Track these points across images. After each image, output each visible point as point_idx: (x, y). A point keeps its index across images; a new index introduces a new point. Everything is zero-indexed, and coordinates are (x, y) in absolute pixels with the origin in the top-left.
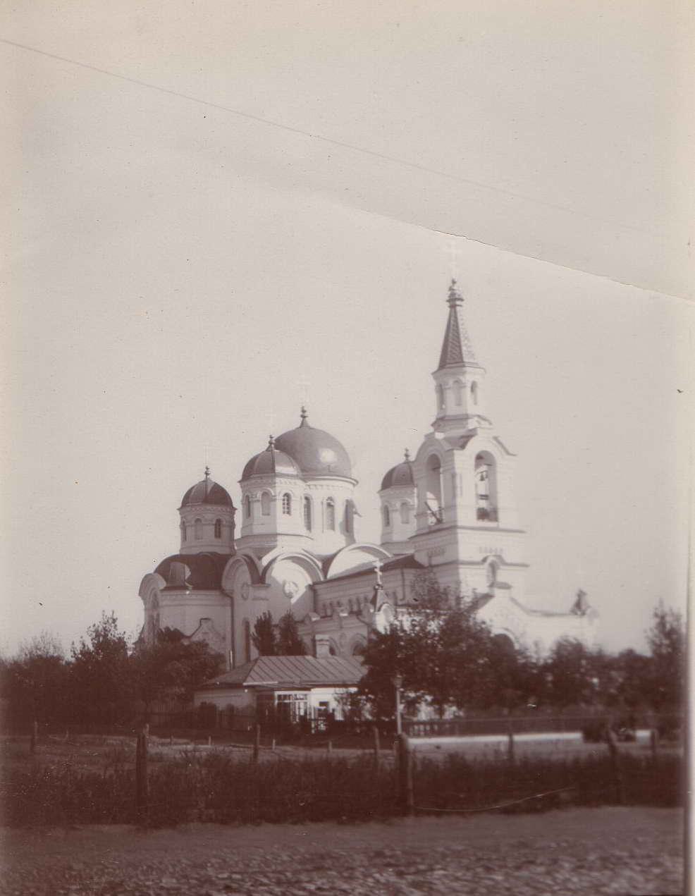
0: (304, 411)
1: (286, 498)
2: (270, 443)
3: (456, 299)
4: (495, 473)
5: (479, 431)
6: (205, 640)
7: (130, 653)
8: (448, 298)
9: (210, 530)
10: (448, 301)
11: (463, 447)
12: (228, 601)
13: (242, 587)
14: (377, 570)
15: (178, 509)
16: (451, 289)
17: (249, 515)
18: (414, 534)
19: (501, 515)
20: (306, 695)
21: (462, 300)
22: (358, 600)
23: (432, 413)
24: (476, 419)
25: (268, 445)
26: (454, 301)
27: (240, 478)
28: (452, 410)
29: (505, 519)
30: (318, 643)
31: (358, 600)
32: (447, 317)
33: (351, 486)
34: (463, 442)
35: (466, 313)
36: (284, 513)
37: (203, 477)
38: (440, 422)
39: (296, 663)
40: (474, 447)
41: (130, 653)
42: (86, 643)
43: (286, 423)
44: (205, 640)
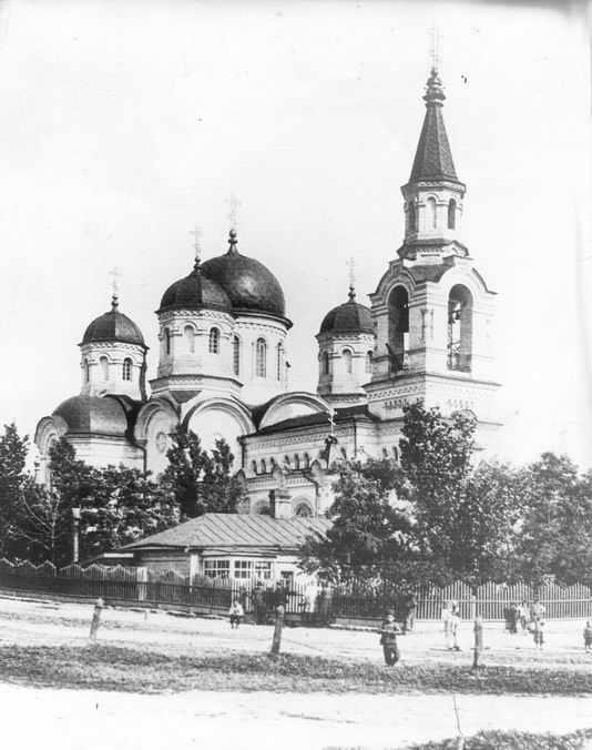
0: (232, 236)
3: (437, 96)
4: (469, 314)
5: (456, 260)
6: (577, 466)
8: (424, 94)
9: (118, 370)
10: (425, 98)
11: (437, 279)
12: (140, 453)
13: (158, 437)
14: (331, 420)
15: (157, 312)
17: (168, 352)
18: (369, 381)
19: (474, 363)
20: (269, 563)
21: (443, 98)
24: (453, 246)
25: (193, 269)
26: (433, 98)
27: (158, 307)
28: (426, 231)
30: (277, 500)
33: (284, 328)
34: (436, 274)
35: (449, 113)
36: (210, 351)
37: (109, 309)
38: (410, 247)
40: (450, 279)
43: (215, 249)
44: (577, 466)
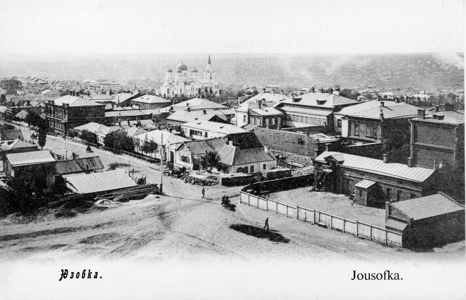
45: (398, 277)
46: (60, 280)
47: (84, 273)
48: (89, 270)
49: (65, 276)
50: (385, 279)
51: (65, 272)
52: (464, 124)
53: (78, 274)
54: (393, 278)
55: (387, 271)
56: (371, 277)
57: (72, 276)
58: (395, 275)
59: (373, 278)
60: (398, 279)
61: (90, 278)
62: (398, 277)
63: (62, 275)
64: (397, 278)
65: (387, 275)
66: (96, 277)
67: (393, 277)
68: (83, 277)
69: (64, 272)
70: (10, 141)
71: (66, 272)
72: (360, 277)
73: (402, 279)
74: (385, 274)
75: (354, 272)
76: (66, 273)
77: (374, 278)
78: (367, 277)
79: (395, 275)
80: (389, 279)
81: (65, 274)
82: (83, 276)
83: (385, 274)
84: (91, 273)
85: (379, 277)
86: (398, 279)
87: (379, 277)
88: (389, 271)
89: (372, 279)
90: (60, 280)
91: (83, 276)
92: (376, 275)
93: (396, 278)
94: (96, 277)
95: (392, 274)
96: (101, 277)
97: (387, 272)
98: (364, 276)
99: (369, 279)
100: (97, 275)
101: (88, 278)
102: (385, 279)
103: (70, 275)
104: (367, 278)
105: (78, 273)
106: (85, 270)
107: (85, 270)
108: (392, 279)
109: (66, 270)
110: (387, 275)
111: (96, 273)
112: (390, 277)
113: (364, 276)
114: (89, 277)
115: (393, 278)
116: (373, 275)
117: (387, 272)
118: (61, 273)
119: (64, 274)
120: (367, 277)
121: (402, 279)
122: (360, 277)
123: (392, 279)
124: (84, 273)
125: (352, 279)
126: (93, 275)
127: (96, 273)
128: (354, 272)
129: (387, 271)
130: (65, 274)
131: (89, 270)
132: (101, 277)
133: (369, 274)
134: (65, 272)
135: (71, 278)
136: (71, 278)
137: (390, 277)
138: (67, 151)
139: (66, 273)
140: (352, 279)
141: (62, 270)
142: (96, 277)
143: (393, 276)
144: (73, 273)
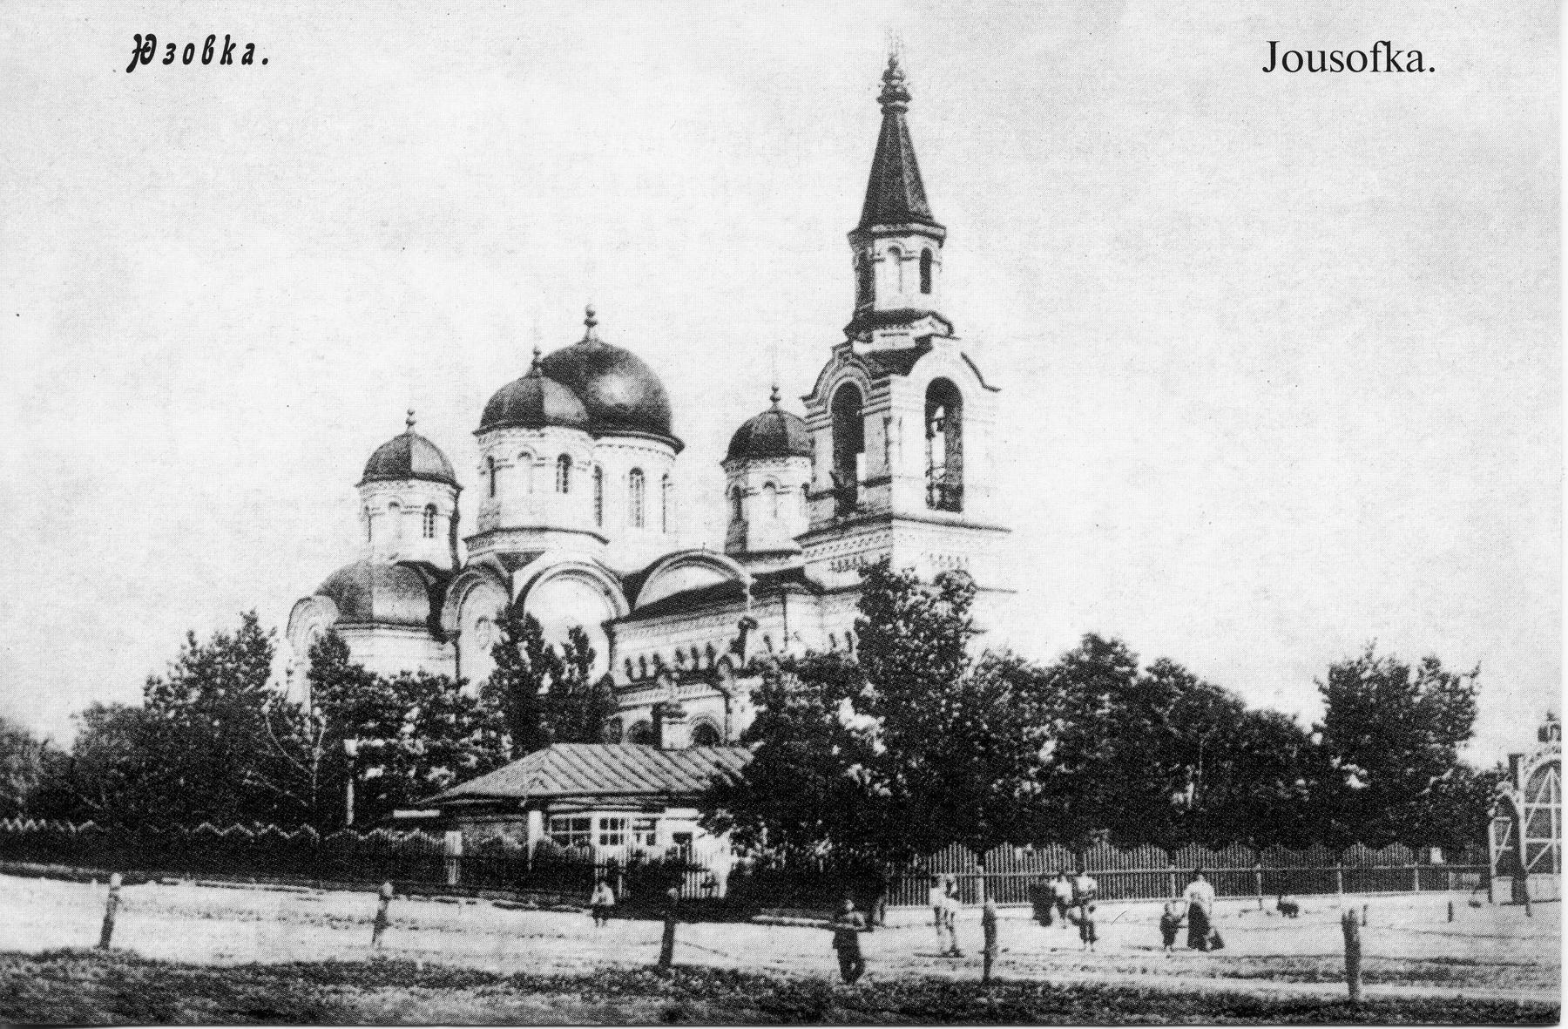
0: (590, 314)
1: (562, 463)
2: (535, 364)
7: (672, 891)
8: (879, 94)
11: (906, 370)
14: (746, 591)
16: (888, 76)
22: (642, 660)
23: (845, 308)
24: (930, 318)
26: (893, 99)
29: (974, 506)
31: (642, 660)
32: (877, 129)
33: (671, 451)
34: (903, 362)
35: (917, 120)
36: (558, 490)
38: (866, 320)
39: (639, 782)
40: (925, 371)
41: (672, 891)
42: (542, 558)
45: (1418, 63)
46: (130, 69)
47: (208, 47)
48: (228, 37)
49: (147, 55)
50: (1375, 69)
51: (147, 44)
52: (1559, 1008)
53: (190, 50)
54: (1404, 68)
55: (1384, 43)
56: (1328, 62)
57: (169, 57)
58: (1409, 55)
59: (1337, 67)
60: (1421, 69)
61: (230, 62)
62: (1418, 63)
63: (136, 52)
64: (1415, 66)
65: (1382, 58)
66: (250, 61)
67: (1403, 64)
68: (206, 61)
69: (144, 42)
70: (1531, 815)
71: (151, 42)
72: (1293, 62)
73: (1432, 70)
74: (1375, 52)
75: (1273, 44)
76: (150, 45)
77: (1338, 68)
78: (1317, 64)
79: (1409, 55)
80: (1389, 69)
81: (146, 49)
82: (207, 57)
83: (1375, 52)
84: (234, 46)
85: (1357, 62)
86: (1421, 69)
87: (1357, 62)
88: (1388, 44)
89: (1332, 70)
90: (130, 69)
91: (207, 57)
92: (1346, 56)
93: (1412, 67)
94: (247, 60)
95: (1399, 52)
96: (265, 61)
97: (1381, 47)
98: (1305, 61)
99: (1323, 69)
100: (251, 53)
101: (223, 62)
102: (1375, 69)
103: (161, 52)
104: (1314, 67)
105: (191, 46)
106: (213, 37)
107: (213, 37)
108: (1400, 70)
109: (151, 37)
110: (1382, 58)
111: (251, 46)
112: (1392, 64)
113: (1305, 61)
114: (227, 59)
115: (1404, 67)
116: (1336, 56)
117: (1381, 47)
118: (134, 45)
119: (144, 50)
120: (1317, 64)
121: (1432, 70)
122: (1293, 62)
123: (1400, 70)
124: (208, 47)
125: (1265, 70)
126: (237, 54)
127: (251, 46)
128: (1273, 44)
129: (1384, 43)
130: (146, 49)
131: (228, 37)
132: (265, 61)
133: (172, 46)
134: (147, 44)
135: (166, 62)
136: (166, 62)
137: (1392, 64)
138: (1227, 928)
139: (150, 45)
140: (1265, 70)
141: (138, 38)
142: (250, 61)
143: (1402, 61)
144: (172, 46)
